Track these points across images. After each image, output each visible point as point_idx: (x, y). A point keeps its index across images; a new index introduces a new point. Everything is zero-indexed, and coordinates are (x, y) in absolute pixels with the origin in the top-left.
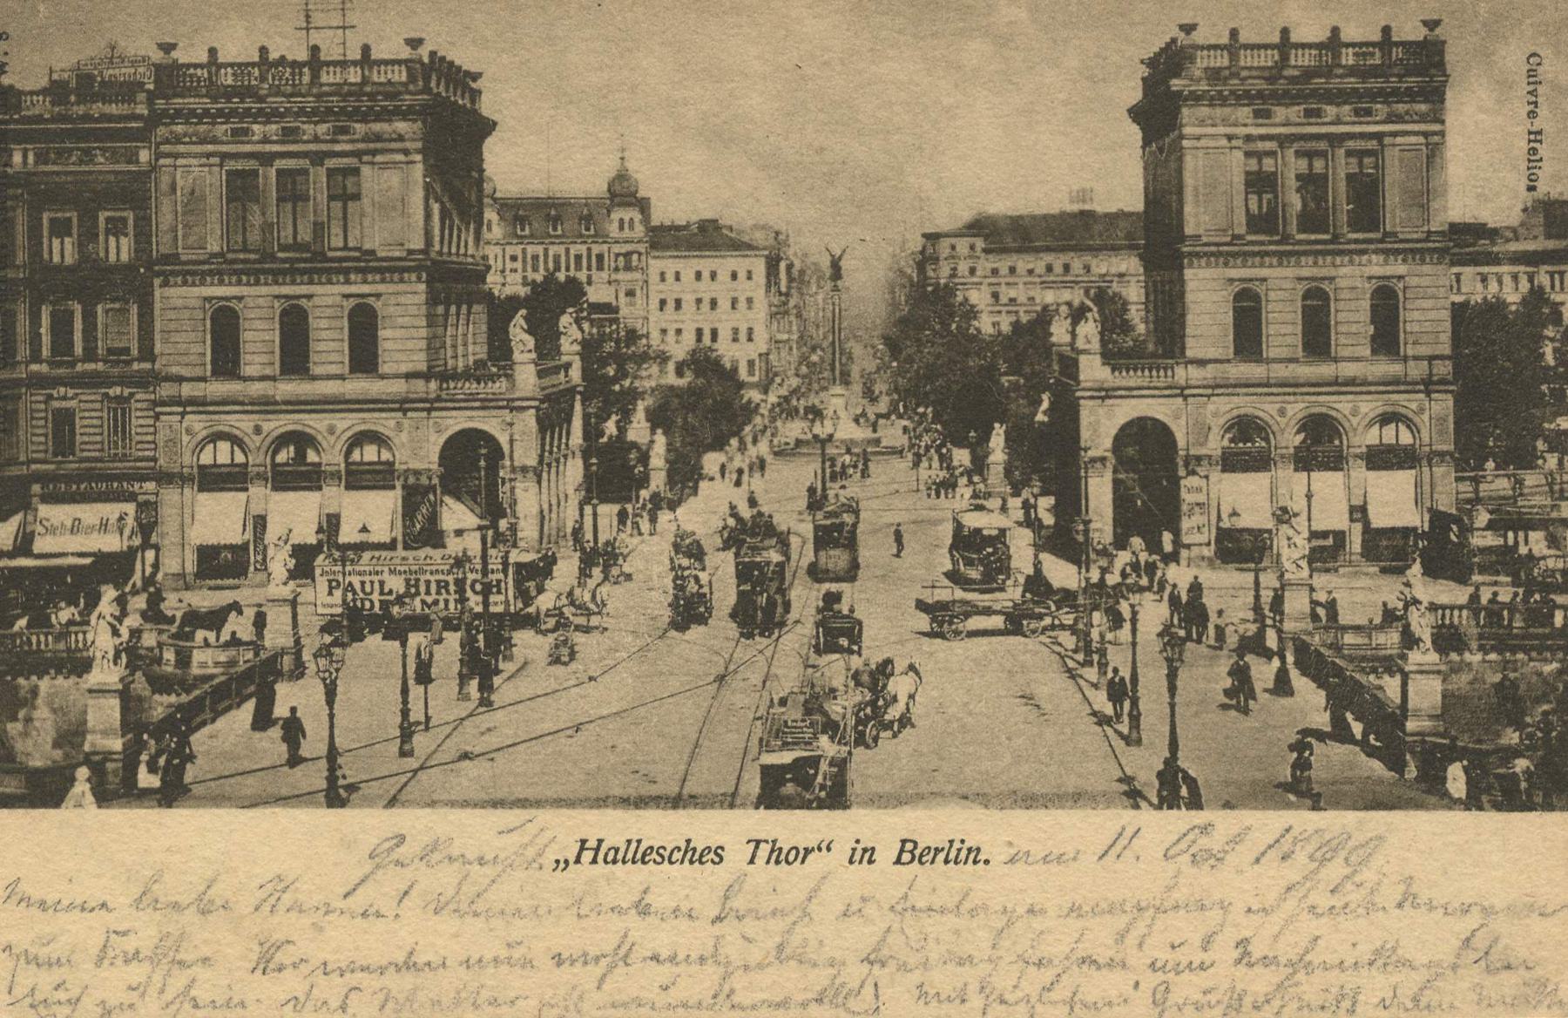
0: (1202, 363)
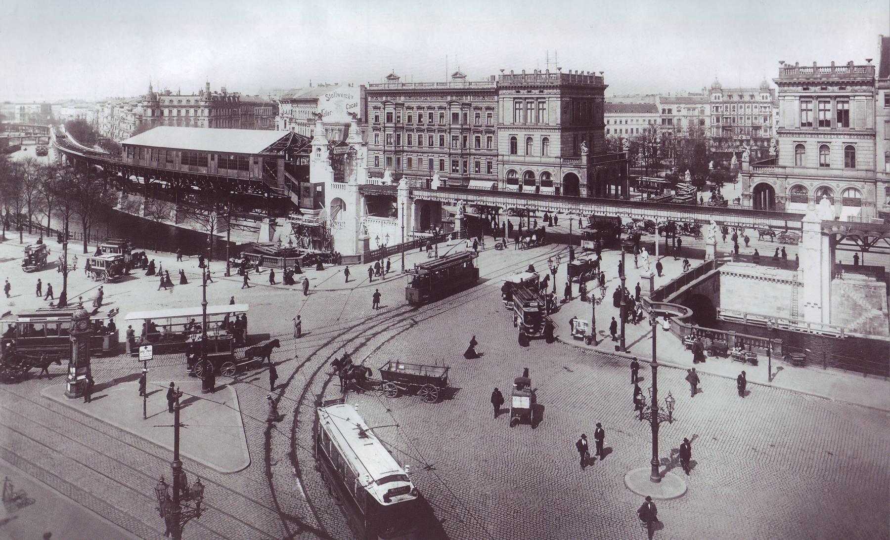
0: (785, 167)
